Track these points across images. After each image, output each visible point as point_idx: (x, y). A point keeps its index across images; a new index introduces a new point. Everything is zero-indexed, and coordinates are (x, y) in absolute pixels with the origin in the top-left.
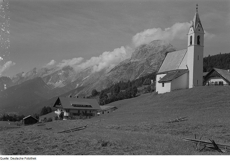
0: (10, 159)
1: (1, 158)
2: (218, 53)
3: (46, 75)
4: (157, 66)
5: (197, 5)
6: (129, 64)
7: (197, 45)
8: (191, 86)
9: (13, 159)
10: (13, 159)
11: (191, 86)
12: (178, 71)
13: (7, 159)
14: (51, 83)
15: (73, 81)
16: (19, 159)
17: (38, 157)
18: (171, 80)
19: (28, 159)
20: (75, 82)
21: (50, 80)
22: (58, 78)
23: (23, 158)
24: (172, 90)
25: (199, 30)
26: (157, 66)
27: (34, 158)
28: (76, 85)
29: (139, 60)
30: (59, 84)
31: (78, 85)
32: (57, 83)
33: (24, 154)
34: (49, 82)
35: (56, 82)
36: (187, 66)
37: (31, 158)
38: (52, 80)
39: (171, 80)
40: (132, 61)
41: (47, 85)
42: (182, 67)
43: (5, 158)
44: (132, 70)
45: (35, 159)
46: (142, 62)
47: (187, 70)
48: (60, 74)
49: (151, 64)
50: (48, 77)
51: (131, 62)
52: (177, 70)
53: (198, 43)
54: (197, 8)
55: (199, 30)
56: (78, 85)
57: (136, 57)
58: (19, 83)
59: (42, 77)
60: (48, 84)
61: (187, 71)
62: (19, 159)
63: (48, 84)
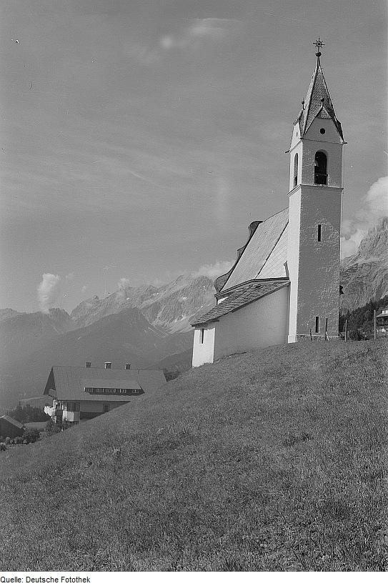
0: (24, 580)
1: (3, 579)
3: (151, 302)
5: (319, 44)
6: (353, 270)
7: (313, 184)
8: (292, 339)
9: (33, 580)
10: (33, 580)
12: (256, 284)
13: (19, 580)
14: (161, 323)
16: (48, 580)
18: (216, 320)
19: (70, 580)
21: (160, 314)
22: (178, 310)
23: (57, 579)
24: (220, 356)
25: (323, 131)
27: (84, 579)
29: (378, 259)
32: (176, 321)
33: (57, 569)
34: (157, 320)
35: (174, 319)
36: (286, 265)
37: (78, 580)
38: (164, 315)
39: (216, 320)
40: (360, 261)
41: (152, 327)
42: (272, 270)
43: (12, 579)
44: (361, 284)
45: (86, 580)
47: (284, 279)
48: (184, 298)
50: (156, 307)
51: (357, 264)
52: (255, 281)
53: (321, 176)
54: (319, 55)
55: (323, 131)
57: (371, 252)
58: (87, 322)
59: (139, 307)
60: (154, 324)
61: (283, 283)
62: (48, 580)
63: (154, 324)
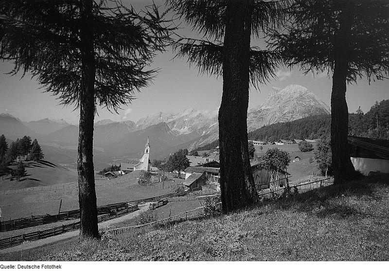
0: (16, 267)
1: (2, 267)
2: (373, 104)
3: (171, 120)
4: (291, 114)
6: (259, 112)
8: (79, 220)
9: (22, 267)
10: (22, 267)
11: (79, 220)
13: (13, 267)
15: (199, 128)
16: (33, 267)
17: (65, 264)
19: (48, 267)
20: (202, 129)
23: (39, 266)
26: (291, 114)
27: (57, 266)
28: (202, 133)
30: (185, 130)
31: (204, 132)
37: (53, 267)
41: (172, 131)
43: (8, 266)
46: (274, 110)
49: (284, 112)
56: (204, 132)
62: (33, 267)
